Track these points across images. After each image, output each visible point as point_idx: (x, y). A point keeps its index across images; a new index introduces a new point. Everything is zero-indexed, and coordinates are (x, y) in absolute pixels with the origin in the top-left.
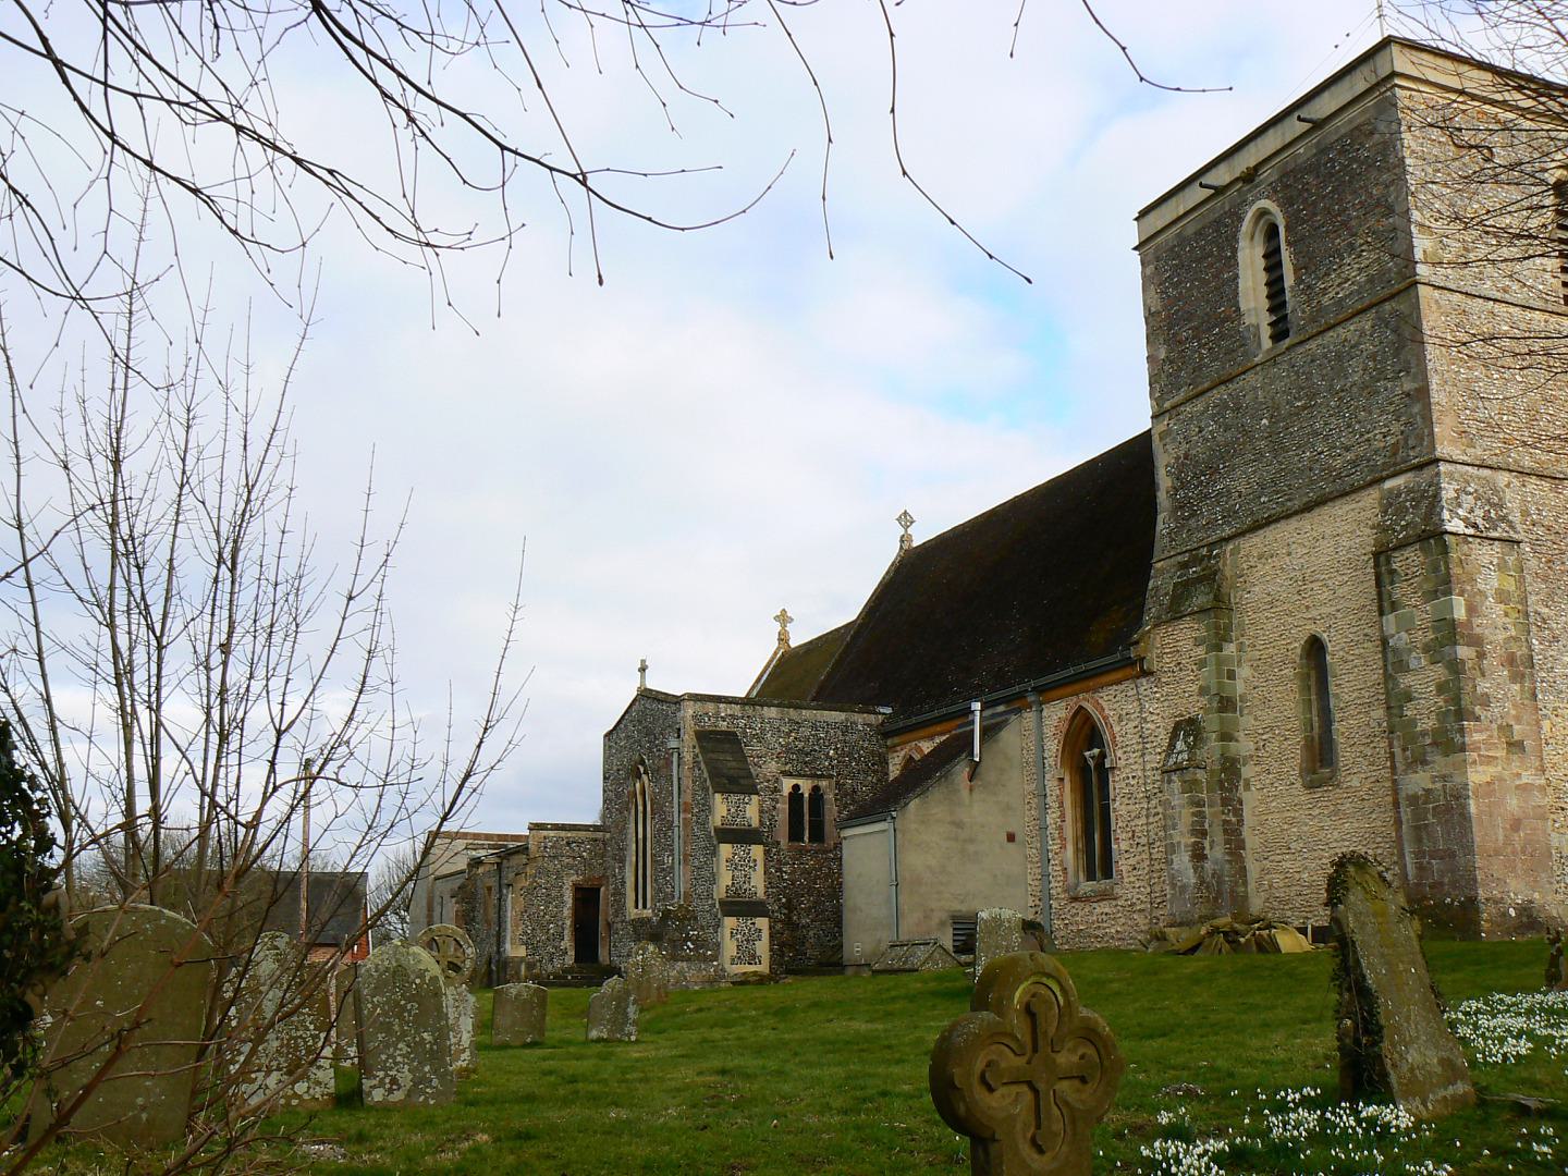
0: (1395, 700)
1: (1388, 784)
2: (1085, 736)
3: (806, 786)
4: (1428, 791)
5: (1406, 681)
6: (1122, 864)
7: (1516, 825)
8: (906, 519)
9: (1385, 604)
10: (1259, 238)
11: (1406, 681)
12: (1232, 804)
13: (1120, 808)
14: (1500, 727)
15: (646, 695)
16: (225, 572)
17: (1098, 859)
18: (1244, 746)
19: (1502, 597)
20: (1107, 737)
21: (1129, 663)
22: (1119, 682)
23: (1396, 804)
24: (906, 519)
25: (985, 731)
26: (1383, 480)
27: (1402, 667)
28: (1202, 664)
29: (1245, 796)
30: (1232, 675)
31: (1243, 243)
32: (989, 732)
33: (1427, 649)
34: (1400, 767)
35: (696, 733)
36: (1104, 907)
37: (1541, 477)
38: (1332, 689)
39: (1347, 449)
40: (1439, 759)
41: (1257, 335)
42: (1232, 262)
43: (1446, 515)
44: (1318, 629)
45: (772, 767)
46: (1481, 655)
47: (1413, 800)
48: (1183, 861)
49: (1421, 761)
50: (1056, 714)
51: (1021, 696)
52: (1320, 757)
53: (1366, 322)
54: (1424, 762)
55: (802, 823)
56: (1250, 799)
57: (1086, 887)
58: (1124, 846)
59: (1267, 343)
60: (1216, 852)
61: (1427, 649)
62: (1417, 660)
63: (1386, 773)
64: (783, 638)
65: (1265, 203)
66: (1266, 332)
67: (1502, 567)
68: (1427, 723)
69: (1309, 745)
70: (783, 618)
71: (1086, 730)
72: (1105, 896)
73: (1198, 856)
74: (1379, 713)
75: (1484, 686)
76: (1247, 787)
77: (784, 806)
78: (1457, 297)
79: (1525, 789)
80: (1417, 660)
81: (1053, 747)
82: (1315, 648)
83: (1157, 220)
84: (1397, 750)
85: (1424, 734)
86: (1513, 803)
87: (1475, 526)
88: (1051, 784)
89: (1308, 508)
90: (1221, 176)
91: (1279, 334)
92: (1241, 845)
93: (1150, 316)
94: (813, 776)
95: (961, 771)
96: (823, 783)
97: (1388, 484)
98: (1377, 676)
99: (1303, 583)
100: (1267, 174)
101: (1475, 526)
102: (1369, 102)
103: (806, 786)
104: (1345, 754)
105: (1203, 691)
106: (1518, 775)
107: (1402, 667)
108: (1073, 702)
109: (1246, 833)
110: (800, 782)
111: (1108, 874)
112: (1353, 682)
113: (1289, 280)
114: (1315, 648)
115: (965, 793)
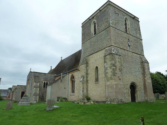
0: (106, 73)
1: (104, 83)
2: (73, 77)
3: (46, 82)
4: (109, 85)
5: (107, 71)
6: (75, 92)
7: (120, 89)
8: (62, 58)
9: (105, 62)
10: (94, 24)
11: (107, 71)
12: (87, 86)
13: (75, 85)
14: (118, 77)
15: (30, 72)
16: (85, 85)
17: (73, 91)
18: (89, 79)
19: (119, 62)
20: (75, 78)
21: (77, 69)
22: (76, 71)
23: (105, 86)
24: (62, 58)
25: (62, 77)
26: (105, 48)
27: (106, 69)
28: (84, 69)
29: (89, 85)
30: (88, 71)
31: (92, 25)
32: (63, 77)
33: (110, 67)
34: (106, 81)
35: (34, 76)
36: (73, 96)
37: (123, 49)
38: (98, 72)
39: (101, 45)
40: (111, 80)
41: (93, 34)
42: (91, 27)
43: (112, 51)
44: (97, 65)
45: (42, 80)
46: (116, 68)
47: (107, 86)
48: (81, 92)
49: (108, 80)
50: (70, 75)
51: (67, 73)
52: (97, 80)
53: (104, 31)
54: (109, 81)
55: (45, 85)
56: (89, 85)
57: (72, 94)
58: (76, 90)
59: (94, 35)
60: (85, 91)
61: (110, 67)
62: (109, 69)
63: (104, 82)
64: (51, 69)
65: (94, 20)
66: (94, 34)
67: (119, 58)
68: (109, 76)
69: (96, 79)
70: (51, 67)
71: (73, 77)
72: (73, 95)
73: (83, 91)
74: (104, 75)
75: (116, 72)
76: (89, 84)
77: (43, 84)
78: (115, 28)
79: (121, 85)
80: (109, 69)
81: (70, 78)
82: (97, 68)
83: (84, 24)
84: (106, 79)
85: (109, 77)
86: (119, 86)
87: (116, 53)
88: (69, 82)
89: (97, 52)
90: (90, 18)
91: (95, 34)
92: (88, 90)
93: (82, 30)
94: (47, 81)
95: (60, 81)
96: (48, 82)
97: (106, 49)
98: (104, 71)
99: (96, 60)
100: (95, 17)
101: (116, 53)
102: (106, 7)
103: (46, 82)
104: (100, 80)
105: (85, 72)
106: (120, 83)
107: (106, 69)
108: (72, 74)
109: (88, 89)
110: (45, 81)
111: (74, 93)
112: (101, 71)
113: (96, 27)
114: (97, 68)
115: (60, 83)
